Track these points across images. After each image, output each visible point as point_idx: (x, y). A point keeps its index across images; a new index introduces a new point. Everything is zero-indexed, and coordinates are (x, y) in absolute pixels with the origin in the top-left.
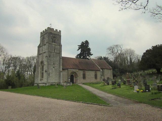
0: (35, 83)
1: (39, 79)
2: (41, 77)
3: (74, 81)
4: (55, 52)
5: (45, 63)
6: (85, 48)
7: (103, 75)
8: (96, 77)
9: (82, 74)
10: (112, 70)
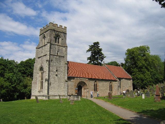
0: (32, 95)
1: (38, 90)
2: (40, 88)
3: (83, 94)
4: (59, 55)
5: (46, 69)
6: (96, 52)
7: (120, 86)
8: (112, 89)
9: (93, 85)
10: (131, 80)
